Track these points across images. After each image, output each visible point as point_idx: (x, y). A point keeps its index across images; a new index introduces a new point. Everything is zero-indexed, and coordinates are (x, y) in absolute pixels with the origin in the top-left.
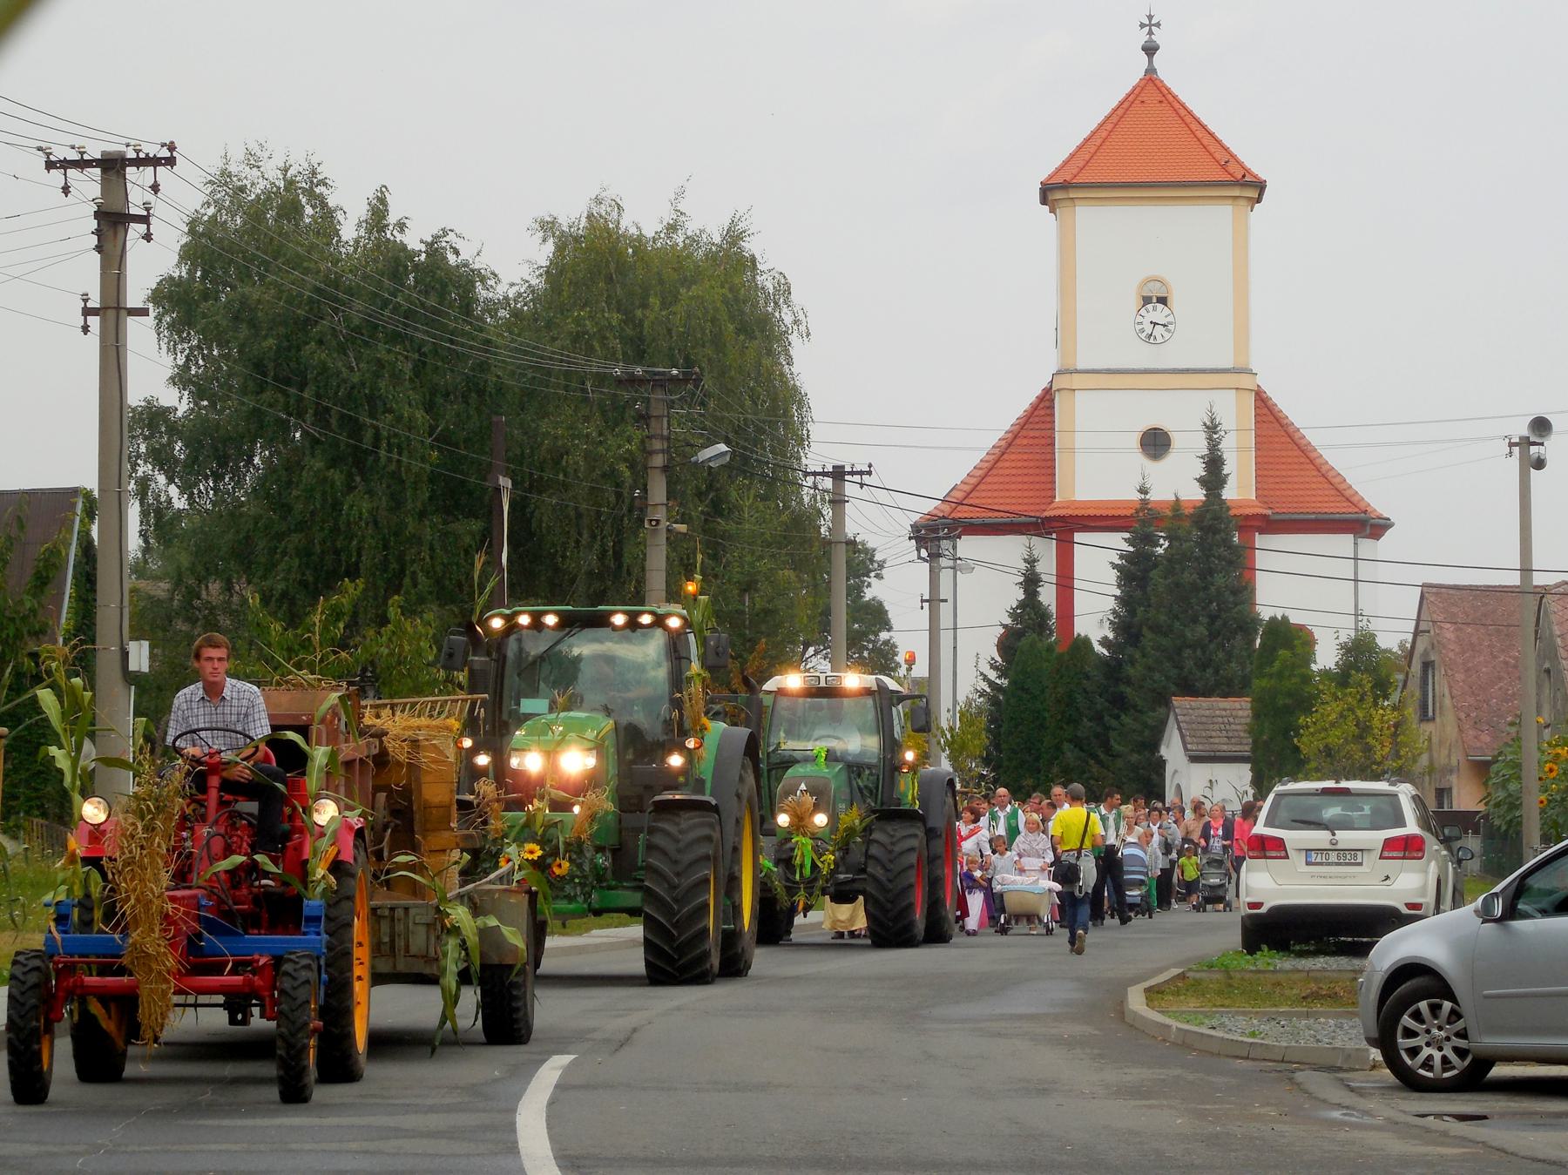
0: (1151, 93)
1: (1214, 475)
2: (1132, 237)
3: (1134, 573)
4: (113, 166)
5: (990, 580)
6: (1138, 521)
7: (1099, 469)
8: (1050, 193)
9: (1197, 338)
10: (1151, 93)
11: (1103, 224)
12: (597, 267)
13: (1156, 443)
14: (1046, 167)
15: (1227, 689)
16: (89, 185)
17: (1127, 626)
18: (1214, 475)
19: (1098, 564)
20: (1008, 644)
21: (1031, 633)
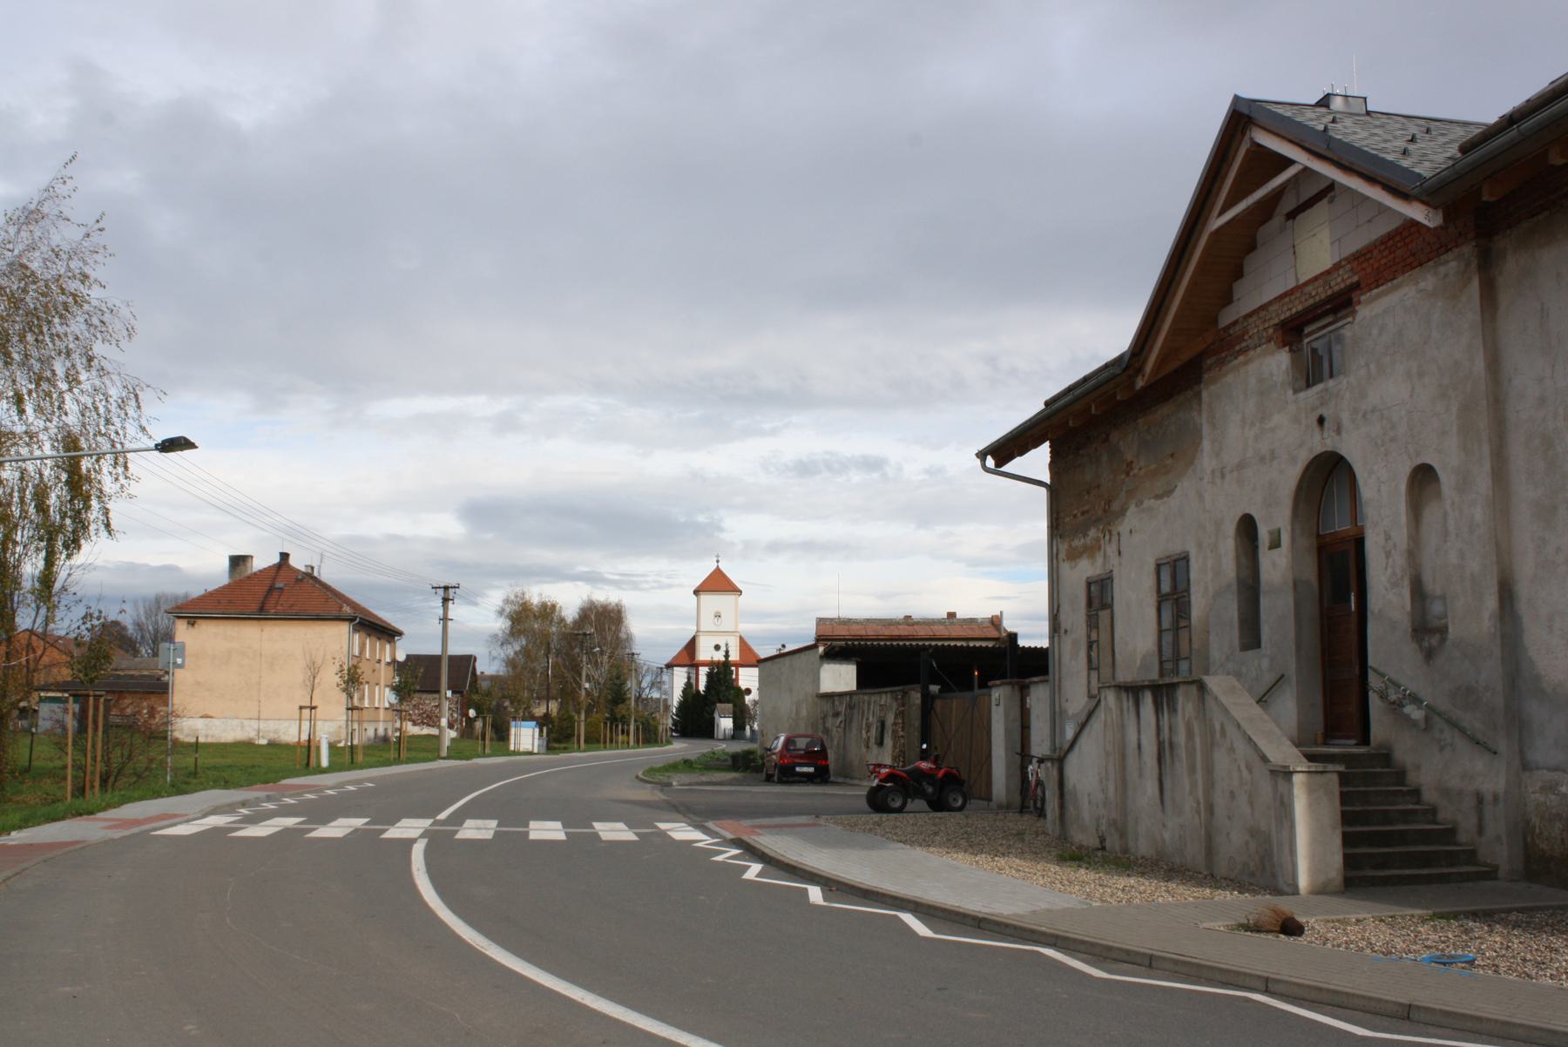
0: (718, 571)
1: (727, 655)
2: (712, 601)
3: (709, 675)
4: (446, 588)
5: (680, 677)
6: (711, 664)
7: (705, 653)
8: (696, 592)
9: (727, 624)
10: (718, 571)
11: (706, 598)
12: (544, 606)
13: (717, 648)
14: (698, 583)
15: (728, 701)
16: (441, 592)
17: (708, 687)
18: (727, 655)
19: (703, 671)
20: (684, 691)
21: (689, 688)
